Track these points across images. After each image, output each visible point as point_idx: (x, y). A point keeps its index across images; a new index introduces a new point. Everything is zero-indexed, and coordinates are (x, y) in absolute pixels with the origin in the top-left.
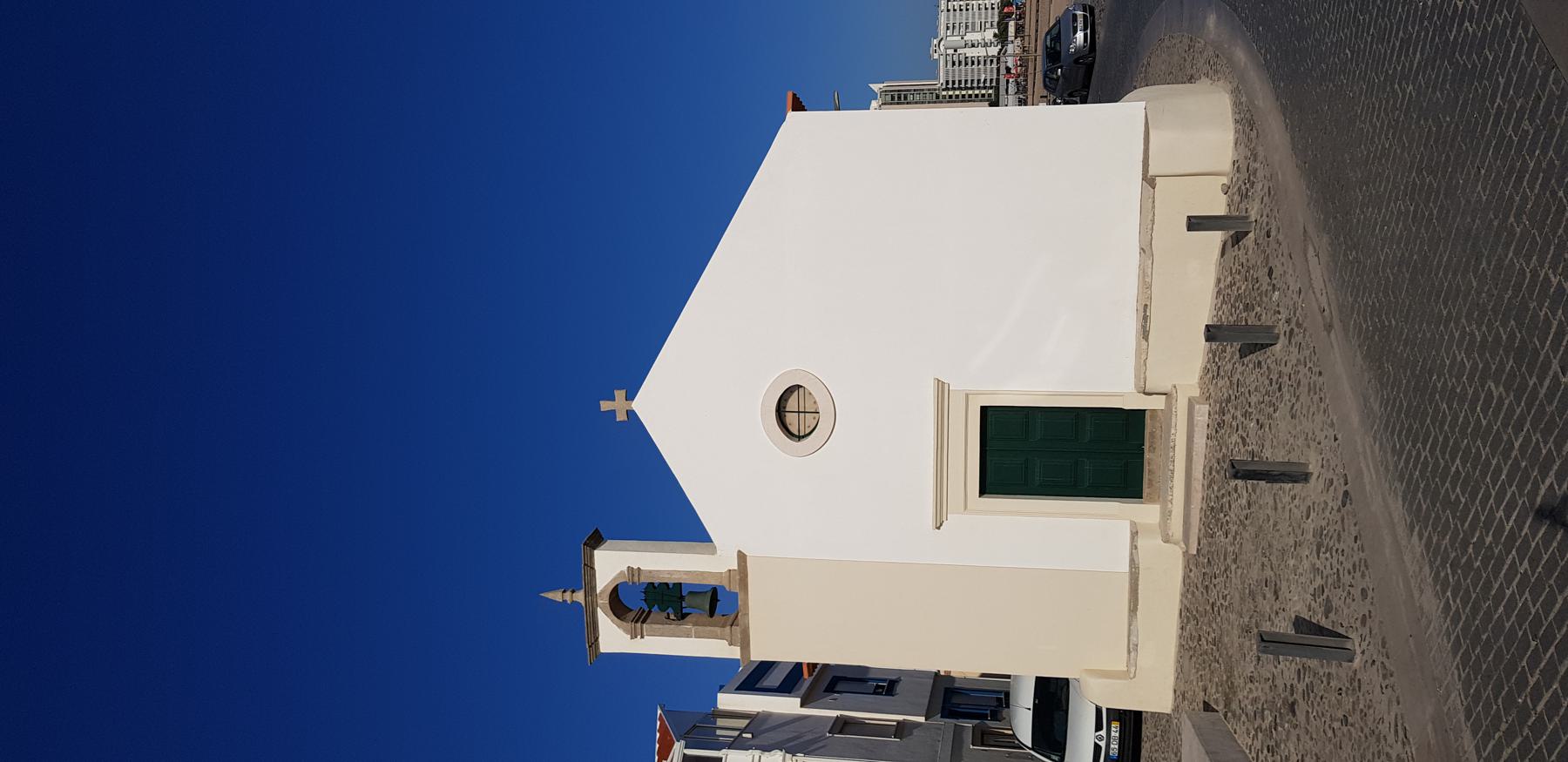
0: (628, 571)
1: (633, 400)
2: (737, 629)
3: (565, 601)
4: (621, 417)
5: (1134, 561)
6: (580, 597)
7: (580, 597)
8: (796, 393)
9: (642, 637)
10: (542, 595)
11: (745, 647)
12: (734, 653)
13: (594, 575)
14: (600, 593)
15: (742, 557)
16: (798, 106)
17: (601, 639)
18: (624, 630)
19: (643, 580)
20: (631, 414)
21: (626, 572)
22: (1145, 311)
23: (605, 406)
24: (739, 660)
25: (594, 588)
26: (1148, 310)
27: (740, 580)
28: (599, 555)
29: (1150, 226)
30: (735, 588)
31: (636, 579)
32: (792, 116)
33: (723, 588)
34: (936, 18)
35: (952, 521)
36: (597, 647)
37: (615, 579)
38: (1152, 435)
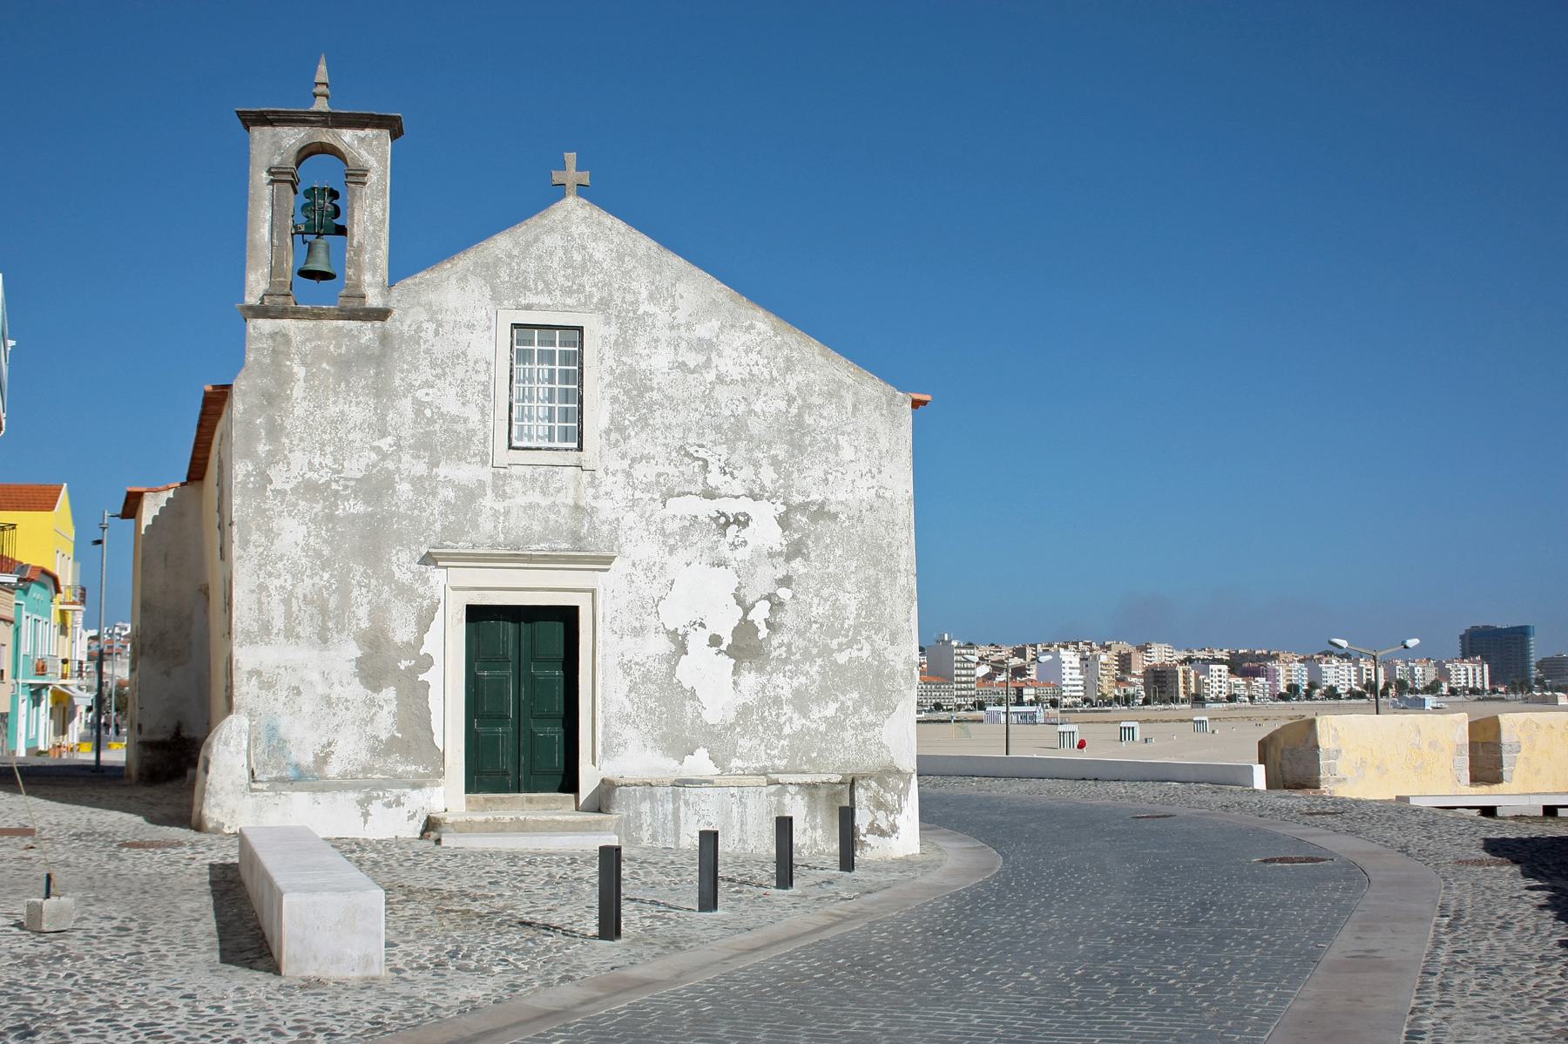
4: (557, 177)
16: (916, 404)
20: (559, 192)
23: (571, 158)
26: (706, 785)
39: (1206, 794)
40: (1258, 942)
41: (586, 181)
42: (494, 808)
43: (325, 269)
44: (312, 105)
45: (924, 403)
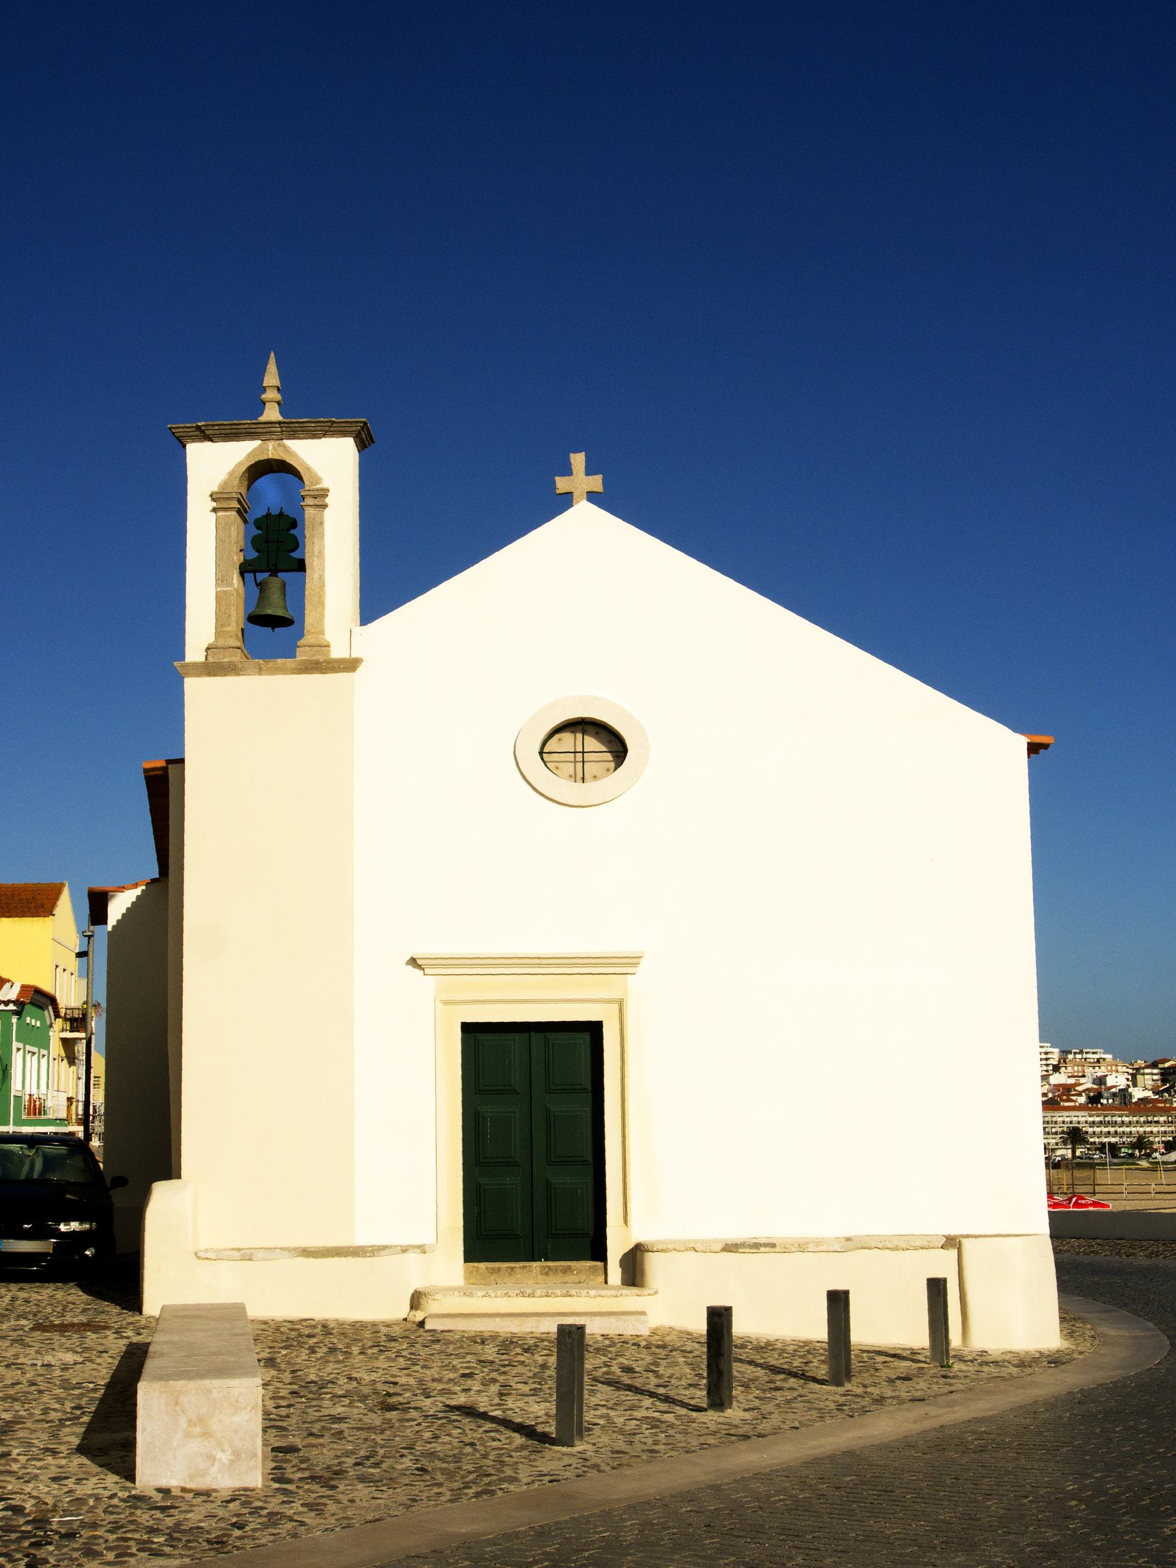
0: (322, 490)
1: (589, 500)
2: (237, 657)
3: (264, 390)
4: (562, 484)
5: (383, 1250)
6: (272, 413)
7: (272, 413)
8: (604, 749)
9: (214, 510)
10: (272, 355)
11: (210, 669)
12: (194, 652)
13: (314, 437)
14: (284, 446)
15: (350, 665)
16: (1033, 749)
17: (208, 445)
18: (225, 483)
19: (309, 512)
20: (565, 502)
21: (318, 486)
22: (766, 1245)
23: (578, 460)
24: (184, 660)
25: (293, 435)
26: (767, 1249)
27: (318, 662)
28: (347, 446)
29: (889, 1245)
30: (302, 655)
31: (309, 501)
32: (1020, 742)
33: (301, 635)
34: (86, 1063)
35: (424, 985)
36: (196, 439)
37: (308, 469)
38: (566, 1271)
39: (546, 1335)
40: (1074, 1503)
41: (598, 487)
42: (499, 1281)
43: (280, 612)
44: (261, 414)
45: (1045, 746)
